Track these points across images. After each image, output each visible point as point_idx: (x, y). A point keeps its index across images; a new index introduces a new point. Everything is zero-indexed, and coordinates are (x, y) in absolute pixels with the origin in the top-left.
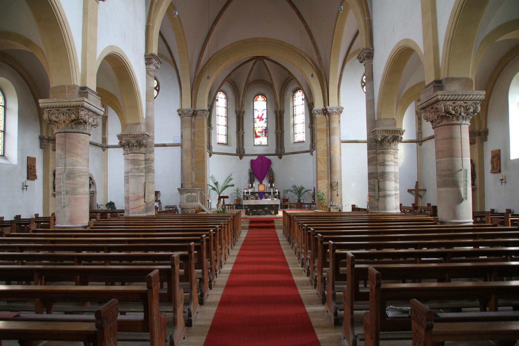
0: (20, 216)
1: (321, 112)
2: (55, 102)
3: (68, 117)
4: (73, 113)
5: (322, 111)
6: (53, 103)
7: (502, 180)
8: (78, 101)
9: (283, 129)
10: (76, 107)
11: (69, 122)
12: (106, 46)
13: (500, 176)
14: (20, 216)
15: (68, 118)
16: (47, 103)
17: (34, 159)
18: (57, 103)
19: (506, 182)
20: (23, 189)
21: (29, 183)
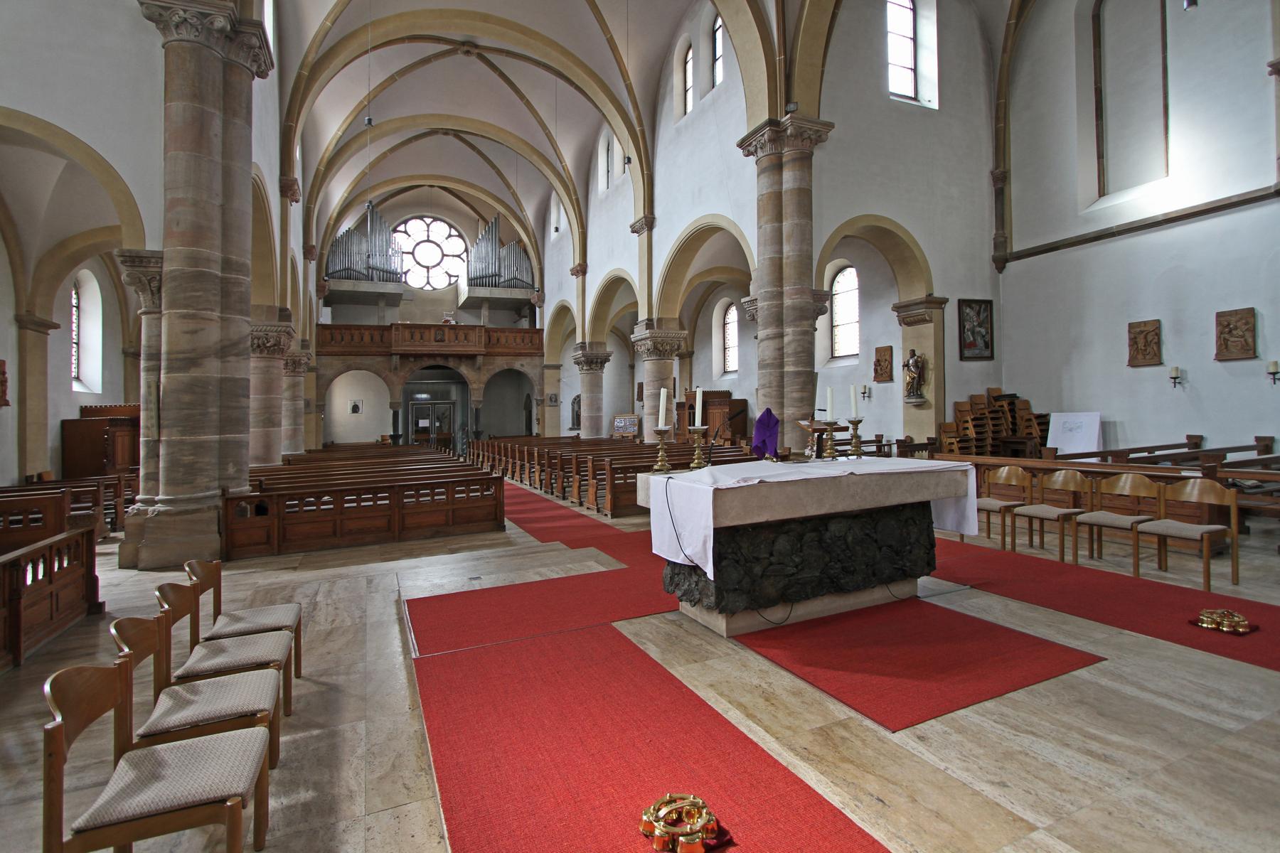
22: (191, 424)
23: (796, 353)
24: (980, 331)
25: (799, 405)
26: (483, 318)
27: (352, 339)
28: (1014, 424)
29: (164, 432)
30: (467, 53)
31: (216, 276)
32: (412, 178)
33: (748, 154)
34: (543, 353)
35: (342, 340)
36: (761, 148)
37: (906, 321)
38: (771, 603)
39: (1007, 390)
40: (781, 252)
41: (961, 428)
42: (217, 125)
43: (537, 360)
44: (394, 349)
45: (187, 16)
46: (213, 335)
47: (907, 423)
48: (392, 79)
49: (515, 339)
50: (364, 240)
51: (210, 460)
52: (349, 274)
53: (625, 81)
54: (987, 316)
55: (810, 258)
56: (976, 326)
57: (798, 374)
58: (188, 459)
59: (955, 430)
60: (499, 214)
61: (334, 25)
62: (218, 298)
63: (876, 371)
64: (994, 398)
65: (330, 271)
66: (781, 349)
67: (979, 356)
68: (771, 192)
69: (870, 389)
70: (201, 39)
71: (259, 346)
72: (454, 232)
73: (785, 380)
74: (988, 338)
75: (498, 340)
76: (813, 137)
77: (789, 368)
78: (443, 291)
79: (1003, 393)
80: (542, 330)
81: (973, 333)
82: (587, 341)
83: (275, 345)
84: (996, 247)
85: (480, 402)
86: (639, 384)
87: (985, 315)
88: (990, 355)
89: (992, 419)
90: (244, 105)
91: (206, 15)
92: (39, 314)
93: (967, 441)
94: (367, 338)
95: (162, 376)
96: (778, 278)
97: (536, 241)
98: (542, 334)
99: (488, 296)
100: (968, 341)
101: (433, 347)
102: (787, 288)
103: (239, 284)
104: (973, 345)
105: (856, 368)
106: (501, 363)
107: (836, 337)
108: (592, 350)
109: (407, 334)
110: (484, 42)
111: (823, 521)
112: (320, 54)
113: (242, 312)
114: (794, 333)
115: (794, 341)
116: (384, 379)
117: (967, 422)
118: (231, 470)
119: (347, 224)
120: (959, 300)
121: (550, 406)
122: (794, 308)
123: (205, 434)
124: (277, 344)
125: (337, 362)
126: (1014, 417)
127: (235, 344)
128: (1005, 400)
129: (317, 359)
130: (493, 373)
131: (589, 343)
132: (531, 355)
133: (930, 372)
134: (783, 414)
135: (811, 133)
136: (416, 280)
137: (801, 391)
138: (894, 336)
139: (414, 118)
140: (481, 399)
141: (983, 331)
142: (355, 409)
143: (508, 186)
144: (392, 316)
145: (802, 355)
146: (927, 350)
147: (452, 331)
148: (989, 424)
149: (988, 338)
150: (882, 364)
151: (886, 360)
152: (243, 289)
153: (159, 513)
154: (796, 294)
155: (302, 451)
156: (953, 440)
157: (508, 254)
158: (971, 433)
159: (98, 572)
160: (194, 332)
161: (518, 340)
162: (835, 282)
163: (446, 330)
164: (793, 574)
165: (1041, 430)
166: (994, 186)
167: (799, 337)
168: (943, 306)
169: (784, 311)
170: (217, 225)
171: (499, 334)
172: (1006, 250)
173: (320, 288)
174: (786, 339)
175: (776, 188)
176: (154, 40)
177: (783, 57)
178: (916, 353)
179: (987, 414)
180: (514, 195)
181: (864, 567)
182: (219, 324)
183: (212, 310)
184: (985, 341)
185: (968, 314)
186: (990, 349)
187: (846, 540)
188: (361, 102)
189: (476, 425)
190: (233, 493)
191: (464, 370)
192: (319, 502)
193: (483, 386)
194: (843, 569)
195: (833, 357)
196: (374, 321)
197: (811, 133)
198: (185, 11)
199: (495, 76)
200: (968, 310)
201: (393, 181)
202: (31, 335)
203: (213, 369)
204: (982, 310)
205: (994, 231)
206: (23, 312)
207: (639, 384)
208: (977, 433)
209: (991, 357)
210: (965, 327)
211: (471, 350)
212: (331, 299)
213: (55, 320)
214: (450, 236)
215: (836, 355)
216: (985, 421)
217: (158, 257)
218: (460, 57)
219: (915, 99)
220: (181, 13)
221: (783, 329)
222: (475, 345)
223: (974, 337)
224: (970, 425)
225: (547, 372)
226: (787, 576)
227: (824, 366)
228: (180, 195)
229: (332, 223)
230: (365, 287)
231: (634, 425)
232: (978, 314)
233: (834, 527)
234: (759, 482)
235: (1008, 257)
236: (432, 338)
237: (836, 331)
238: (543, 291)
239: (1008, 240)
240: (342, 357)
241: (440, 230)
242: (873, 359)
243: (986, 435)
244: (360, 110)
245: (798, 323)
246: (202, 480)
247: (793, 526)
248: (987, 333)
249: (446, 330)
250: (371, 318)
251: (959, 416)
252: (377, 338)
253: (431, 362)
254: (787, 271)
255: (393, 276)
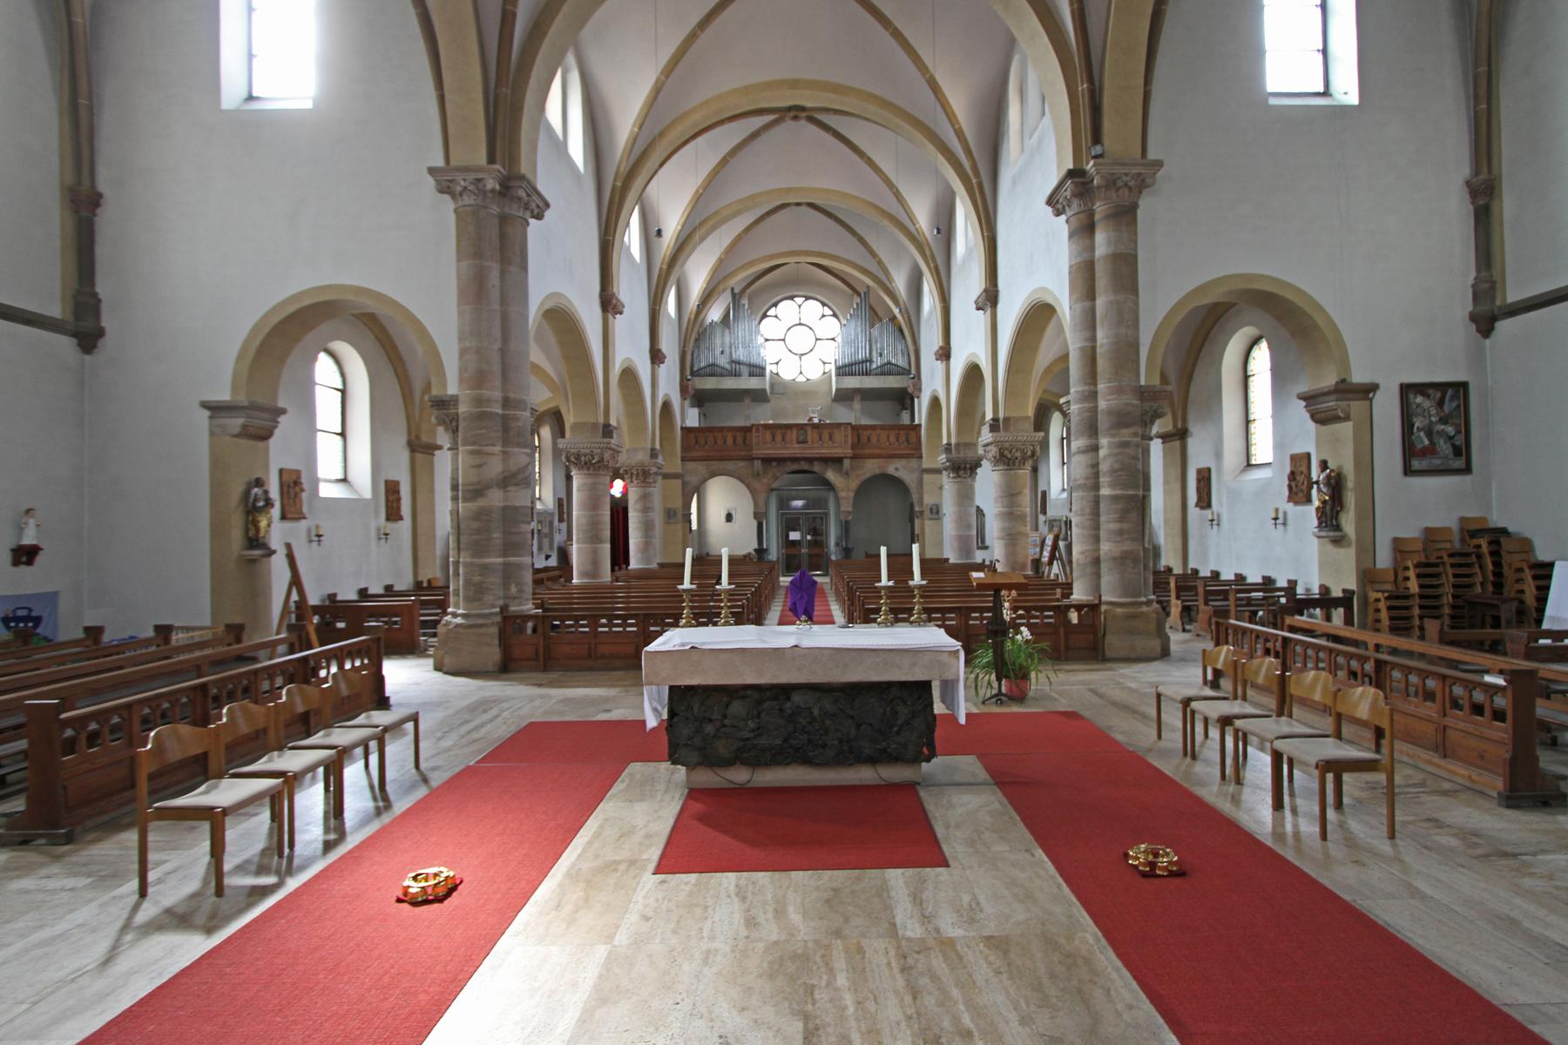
0: (335, 595)
7: (1212, 520)
12: (624, 357)
13: (1208, 513)
14: (335, 595)
17: (397, 483)
19: (1218, 525)
20: (380, 539)
21: (391, 527)
22: (479, 549)
23: (1113, 471)
24: (1443, 430)
25: (1118, 539)
26: (847, 415)
27: (716, 443)
28: (1498, 574)
29: (462, 554)
30: (795, 118)
31: (497, 414)
32: (772, 257)
33: (1058, 213)
34: (921, 454)
35: (706, 443)
36: (1069, 206)
37: (1320, 419)
38: (727, 763)
39: (1497, 520)
40: (1093, 339)
41: (1400, 578)
42: (494, 277)
43: (914, 463)
44: (756, 452)
45: (466, 184)
46: (495, 468)
47: (1323, 565)
48: (724, 162)
49: (888, 437)
50: (727, 332)
51: (495, 580)
52: (713, 371)
53: (953, 126)
54: (1459, 406)
55: (1134, 346)
56: (1436, 423)
57: (1115, 498)
58: (477, 579)
59: (1392, 579)
60: (868, 287)
61: (643, 129)
62: (499, 434)
63: (1290, 487)
64: (1468, 531)
65: (695, 369)
66: (1095, 466)
67: (1441, 468)
68: (1080, 263)
69: (1285, 514)
70: (479, 201)
71: (586, 463)
72: (828, 311)
73: (1102, 505)
74: (1460, 441)
75: (869, 440)
76: (1132, 183)
77: (1105, 491)
78: (818, 383)
79: (1492, 526)
80: (920, 425)
81: (1429, 434)
82: (953, 441)
83: (599, 462)
84: (1476, 298)
85: (849, 513)
86: (1199, 471)
87: (1454, 405)
88: (1464, 466)
89: (1453, 566)
90: (518, 253)
91: (479, 180)
92: (425, 438)
93: (1407, 597)
94: (730, 441)
95: (460, 505)
96: (1091, 375)
97: (909, 317)
98: (920, 430)
99: (858, 386)
100: (1419, 446)
101: (794, 450)
102: (1101, 386)
103: (516, 419)
104: (1430, 451)
105: (1268, 482)
106: (871, 467)
107: (1253, 436)
108: (959, 453)
109: (768, 436)
110: (808, 104)
111: (785, 690)
112: (630, 164)
113: (519, 445)
114: (1110, 445)
115: (1109, 455)
116: (748, 486)
117: (1407, 568)
118: (513, 590)
119: (715, 314)
120: (1401, 385)
121: (931, 519)
122: (1110, 412)
123: (490, 557)
124: (601, 460)
125: (700, 468)
126: (1497, 564)
127: (514, 475)
128: (1483, 537)
129: (683, 465)
130: (863, 478)
131: (956, 444)
132: (907, 456)
133: (1349, 493)
134: (1099, 550)
135: (1128, 178)
136: (788, 372)
137: (1120, 522)
138: (1307, 437)
139: (753, 197)
140: (850, 509)
141: (1450, 430)
142: (729, 518)
143: (873, 254)
144: (762, 415)
145: (1120, 473)
146: (1344, 460)
147: (815, 431)
148: (1446, 574)
149: (1460, 441)
150: (1298, 478)
151: (1302, 473)
152: (520, 424)
153: (457, 626)
154: (1111, 394)
155: (654, 566)
156: (1380, 595)
157: (881, 333)
158: (1413, 586)
159: (385, 672)
160: (479, 466)
161: (892, 439)
162: (1251, 359)
163: (809, 430)
164: (748, 739)
165: (1538, 588)
166: (1473, 203)
167: (1116, 451)
168: (1371, 395)
169: (1099, 416)
170: (497, 368)
171: (869, 432)
172: (1493, 300)
173: (684, 390)
174: (1102, 453)
175: (1086, 256)
176: (448, 205)
177: (1085, 86)
178: (1329, 464)
179: (1446, 558)
180: (880, 263)
181: (836, 742)
182: (501, 457)
183: (493, 445)
184: (1454, 446)
185: (1418, 406)
186: (1464, 457)
187: (811, 713)
188: (697, 191)
189: (846, 541)
190: (514, 611)
191: (831, 475)
192: (577, 625)
193: (852, 494)
194: (810, 741)
195: (1249, 465)
196: (739, 422)
197: (1128, 178)
198: (464, 180)
199: (829, 138)
200: (1419, 399)
201: (752, 263)
202: (419, 456)
203: (495, 498)
204: (1447, 398)
205: (1473, 274)
206: (413, 438)
207: (1199, 471)
208: (1421, 586)
209: (1467, 470)
210: (1413, 425)
211: (836, 451)
212: (700, 399)
213: (439, 443)
214: (823, 316)
215: (1253, 462)
216: (1440, 569)
217: (455, 400)
218: (789, 125)
219: (1326, 93)
220: (462, 183)
221: (1097, 439)
222: (840, 446)
223: (1430, 440)
224: (1411, 574)
225: (926, 477)
226: (742, 740)
227: (1236, 477)
228: (468, 345)
229: (693, 317)
230: (729, 383)
231: (1035, 546)
232: (1440, 404)
233: (797, 698)
234: (692, 647)
235: (1496, 313)
236: (795, 440)
237: (1253, 427)
238: (919, 378)
239: (1498, 286)
240: (705, 463)
241: (812, 309)
242: (1288, 471)
243: (1441, 591)
244: (698, 200)
245: (1113, 432)
246: (489, 598)
247: (749, 692)
248: (1458, 432)
249: (809, 430)
250: (739, 417)
251: (1399, 559)
252: (740, 441)
253: (796, 467)
254: (1102, 364)
255: (758, 370)
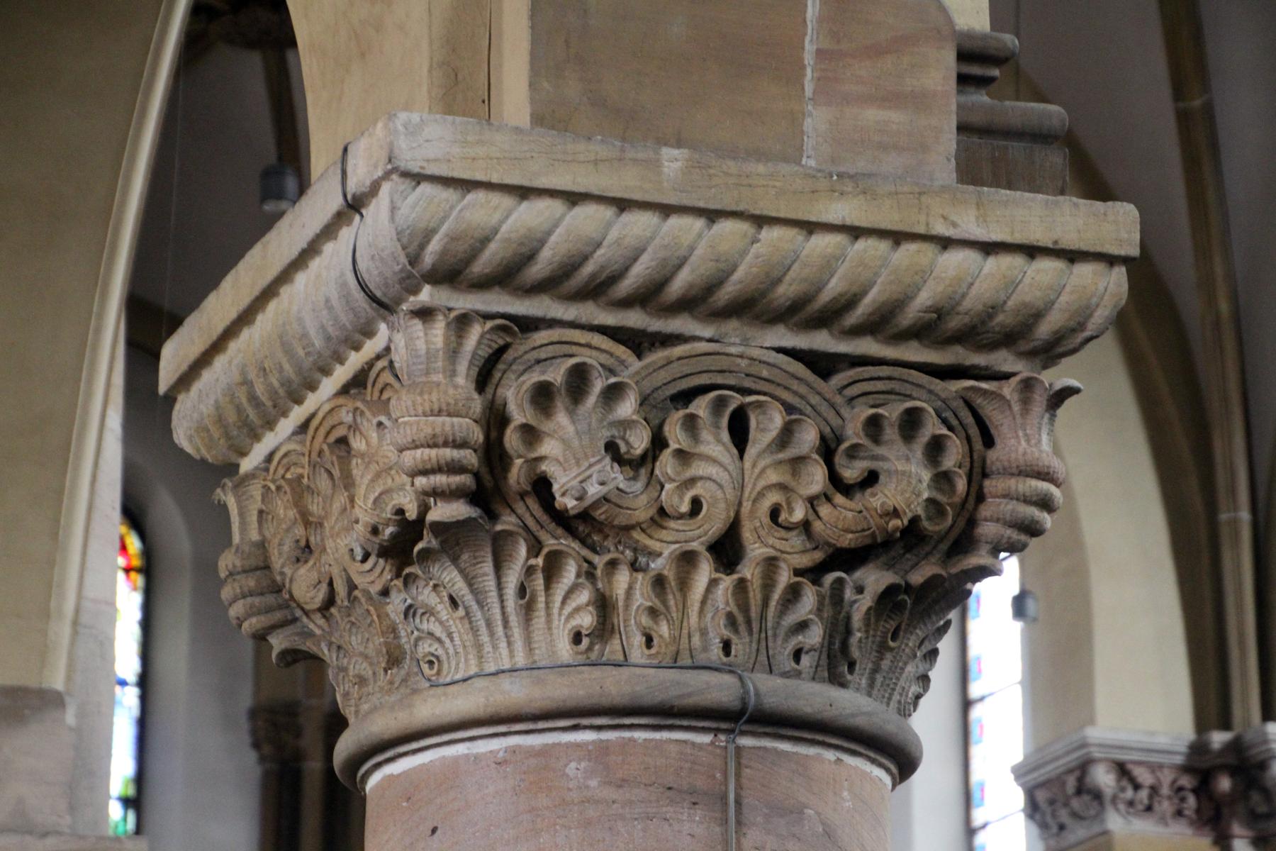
1: (1167, 777)
2: (666, 210)
3: (816, 479)
4: (935, 448)
5: (1186, 769)
6: (622, 205)
8: (1031, 251)
9: (266, 775)
10: (971, 335)
11: (805, 561)
15: (812, 501)
16: (524, 193)
18: (684, 228)
